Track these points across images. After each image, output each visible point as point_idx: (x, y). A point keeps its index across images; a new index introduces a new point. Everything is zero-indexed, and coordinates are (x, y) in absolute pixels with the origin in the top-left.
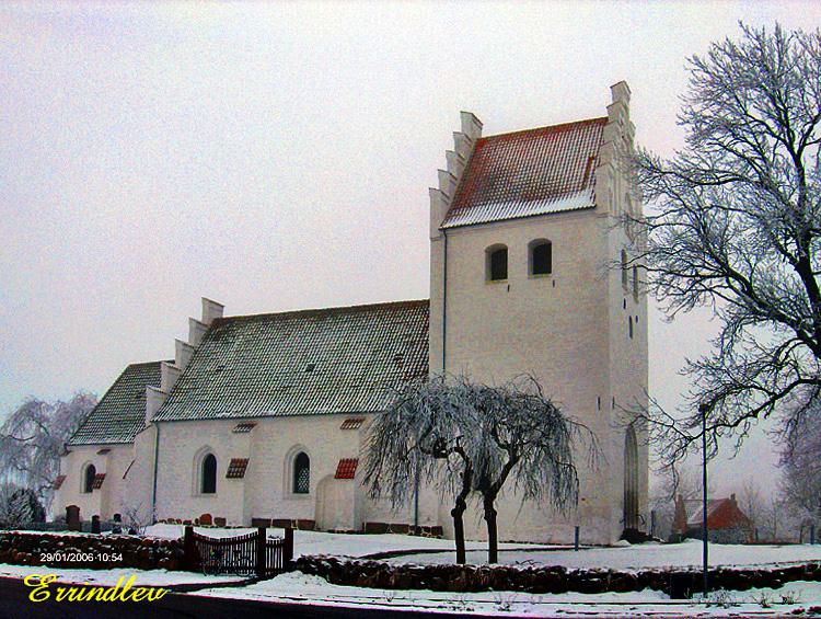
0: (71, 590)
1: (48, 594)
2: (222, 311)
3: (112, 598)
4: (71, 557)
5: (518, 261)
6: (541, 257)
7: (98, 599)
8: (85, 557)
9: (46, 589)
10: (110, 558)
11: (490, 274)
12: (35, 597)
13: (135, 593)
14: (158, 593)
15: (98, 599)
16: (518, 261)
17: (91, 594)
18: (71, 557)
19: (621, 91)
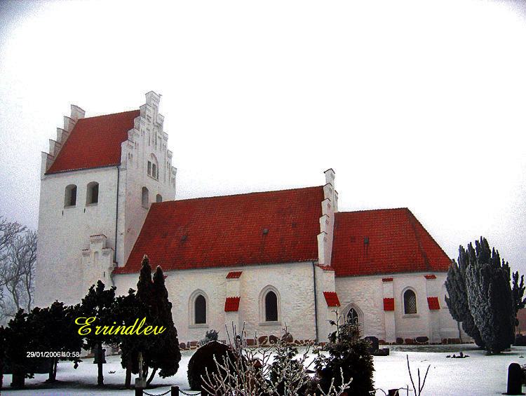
0: (105, 327)
1: (90, 330)
2: (84, 114)
3: (131, 333)
4: (46, 354)
5: (82, 195)
6: (94, 192)
7: (122, 333)
8: (55, 354)
9: (88, 327)
10: (71, 355)
11: (91, 198)
12: (82, 332)
13: (146, 329)
14: (160, 330)
15: (122, 333)
16: (82, 195)
17: (118, 330)
18: (46, 354)
19: (330, 173)
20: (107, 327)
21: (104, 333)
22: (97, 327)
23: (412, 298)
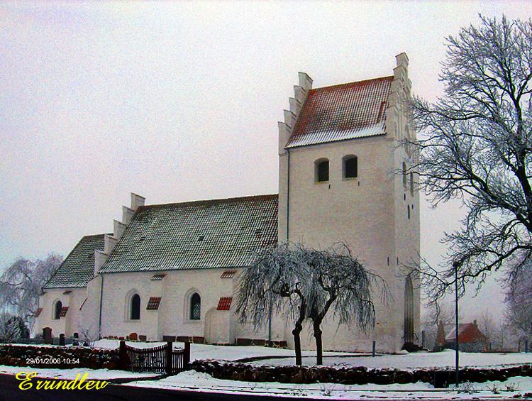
0: (46, 382)
1: (31, 385)
3: (73, 388)
4: (46, 361)
5: (336, 169)
6: (351, 167)
7: (63, 388)
8: (55, 361)
9: (29, 382)
10: (71, 362)
11: (317, 177)
12: (23, 387)
13: (88, 384)
14: (102, 384)
15: (63, 388)
16: (336, 169)
18: (46, 361)
19: (402, 59)
20: (49, 382)
21: (46, 388)
22: (38, 382)
23: (328, 102)
